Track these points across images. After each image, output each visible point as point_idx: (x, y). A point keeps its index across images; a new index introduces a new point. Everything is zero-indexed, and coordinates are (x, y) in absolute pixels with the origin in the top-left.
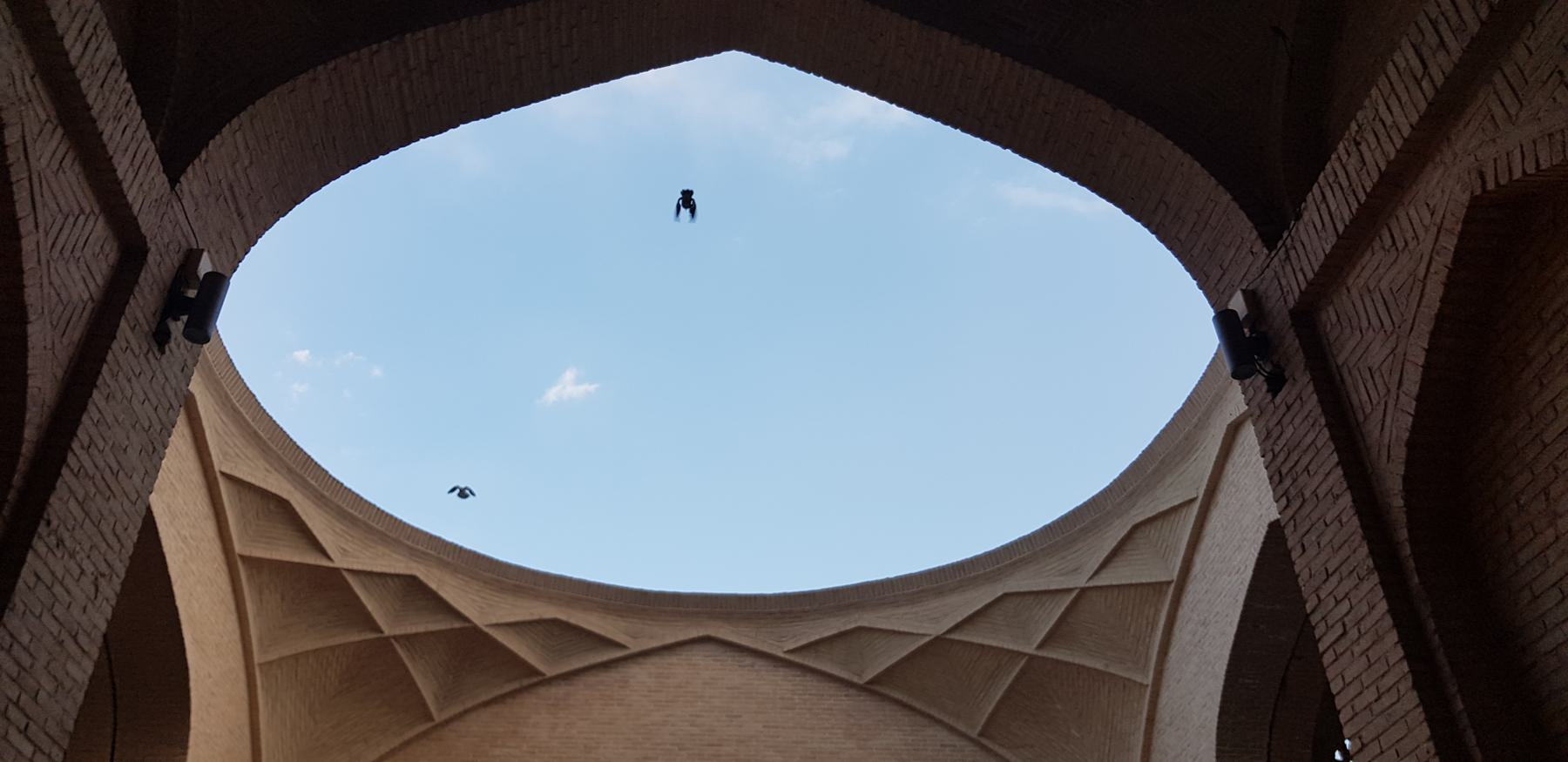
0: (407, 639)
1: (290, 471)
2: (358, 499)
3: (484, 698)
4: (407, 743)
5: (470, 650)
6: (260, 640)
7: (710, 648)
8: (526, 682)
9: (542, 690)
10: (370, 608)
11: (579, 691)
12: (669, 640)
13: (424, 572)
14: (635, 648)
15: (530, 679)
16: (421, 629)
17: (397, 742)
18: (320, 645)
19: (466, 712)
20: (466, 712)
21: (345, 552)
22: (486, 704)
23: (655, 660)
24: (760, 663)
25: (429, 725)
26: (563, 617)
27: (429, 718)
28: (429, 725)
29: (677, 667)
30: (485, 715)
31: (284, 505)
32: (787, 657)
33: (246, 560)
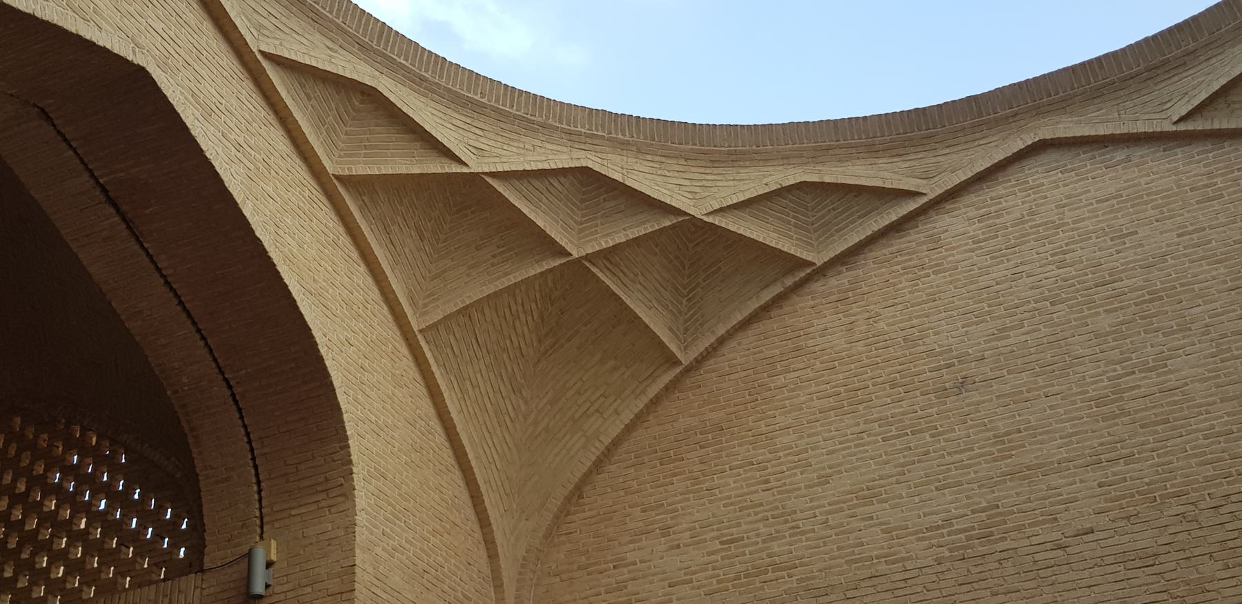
0: (606, 255)
1: (364, 47)
2: (474, 78)
3: (738, 317)
4: (655, 402)
5: (697, 253)
6: (411, 299)
7: (1051, 157)
8: (789, 281)
9: (817, 286)
10: (540, 223)
11: (872, 271)
12: (982, 165)
13: (597, 164)
14: (933, 190)
15: (796, 276)
16: (620, 238)
17: (641, 404)
18: (491, 289)
19: (721, 341)
20: (721, 341)
21: (483, 152)
22: (731, 334)
23: (970, 198)
24: (1138, 153)
25: (678, 370)
26: (815, 178)
27: (677, 362)
28: (678, 370)
29: (1008, 197)
30: (749, 338)
31: (370, 95)
32: (1182, 127)
33: (349, 181)
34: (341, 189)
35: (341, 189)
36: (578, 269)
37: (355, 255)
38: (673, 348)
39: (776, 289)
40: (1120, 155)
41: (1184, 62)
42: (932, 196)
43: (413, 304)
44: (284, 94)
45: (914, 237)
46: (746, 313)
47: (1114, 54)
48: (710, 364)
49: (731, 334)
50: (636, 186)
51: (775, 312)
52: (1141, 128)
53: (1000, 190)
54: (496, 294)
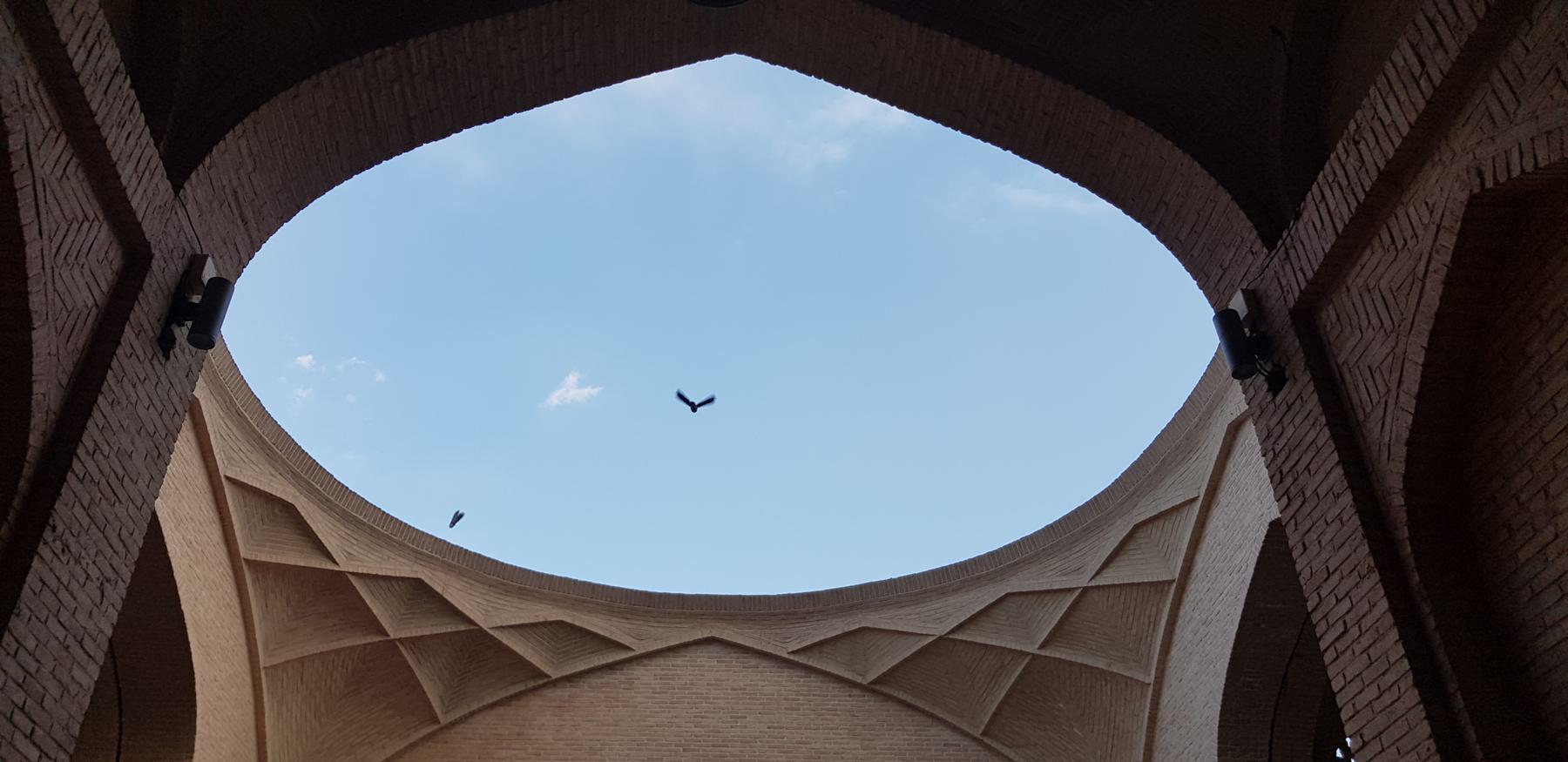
0: (413, 642)
1: (295, 475)
3: (489, 700)
4: (412, 746)
5: (476, 652)
8: (531, 684)
9: (548, 693)
11: (585, 692)
13: (430, 575)
15: (533, 681)
16: (427, 633)
17: (402, 745)
18: (326, 648)
19: (473, 714)
20: (473, 714)
21: (351, 556)
22: (480, 710)
23: (660, 661)
25: (437, 727)
27: (436, 721)
28: (437, 727)
29: (683, 668)
30: (490, 718)
31: (289, 510)
32: (792, 657)
34: (245, 568)
35: (245, 568)
36: (392, 645)
37: (238, 611)
38: (438, 711)
39: (521, 687)
40: (753, 662)
41: (803, 617)
42: (637, 653)
43: (266, 647)
44: (231, 509)
45: (618, 677)
46: (495, 699)
47: (768, 597)
48: (459, 728)
49: (480, 710)
50: (449, 599)
51: (514, 702)
52: (769, 649)
53: (679, 661)
54: (328, 652)
